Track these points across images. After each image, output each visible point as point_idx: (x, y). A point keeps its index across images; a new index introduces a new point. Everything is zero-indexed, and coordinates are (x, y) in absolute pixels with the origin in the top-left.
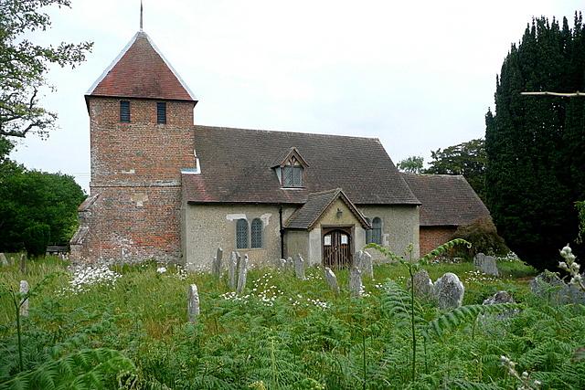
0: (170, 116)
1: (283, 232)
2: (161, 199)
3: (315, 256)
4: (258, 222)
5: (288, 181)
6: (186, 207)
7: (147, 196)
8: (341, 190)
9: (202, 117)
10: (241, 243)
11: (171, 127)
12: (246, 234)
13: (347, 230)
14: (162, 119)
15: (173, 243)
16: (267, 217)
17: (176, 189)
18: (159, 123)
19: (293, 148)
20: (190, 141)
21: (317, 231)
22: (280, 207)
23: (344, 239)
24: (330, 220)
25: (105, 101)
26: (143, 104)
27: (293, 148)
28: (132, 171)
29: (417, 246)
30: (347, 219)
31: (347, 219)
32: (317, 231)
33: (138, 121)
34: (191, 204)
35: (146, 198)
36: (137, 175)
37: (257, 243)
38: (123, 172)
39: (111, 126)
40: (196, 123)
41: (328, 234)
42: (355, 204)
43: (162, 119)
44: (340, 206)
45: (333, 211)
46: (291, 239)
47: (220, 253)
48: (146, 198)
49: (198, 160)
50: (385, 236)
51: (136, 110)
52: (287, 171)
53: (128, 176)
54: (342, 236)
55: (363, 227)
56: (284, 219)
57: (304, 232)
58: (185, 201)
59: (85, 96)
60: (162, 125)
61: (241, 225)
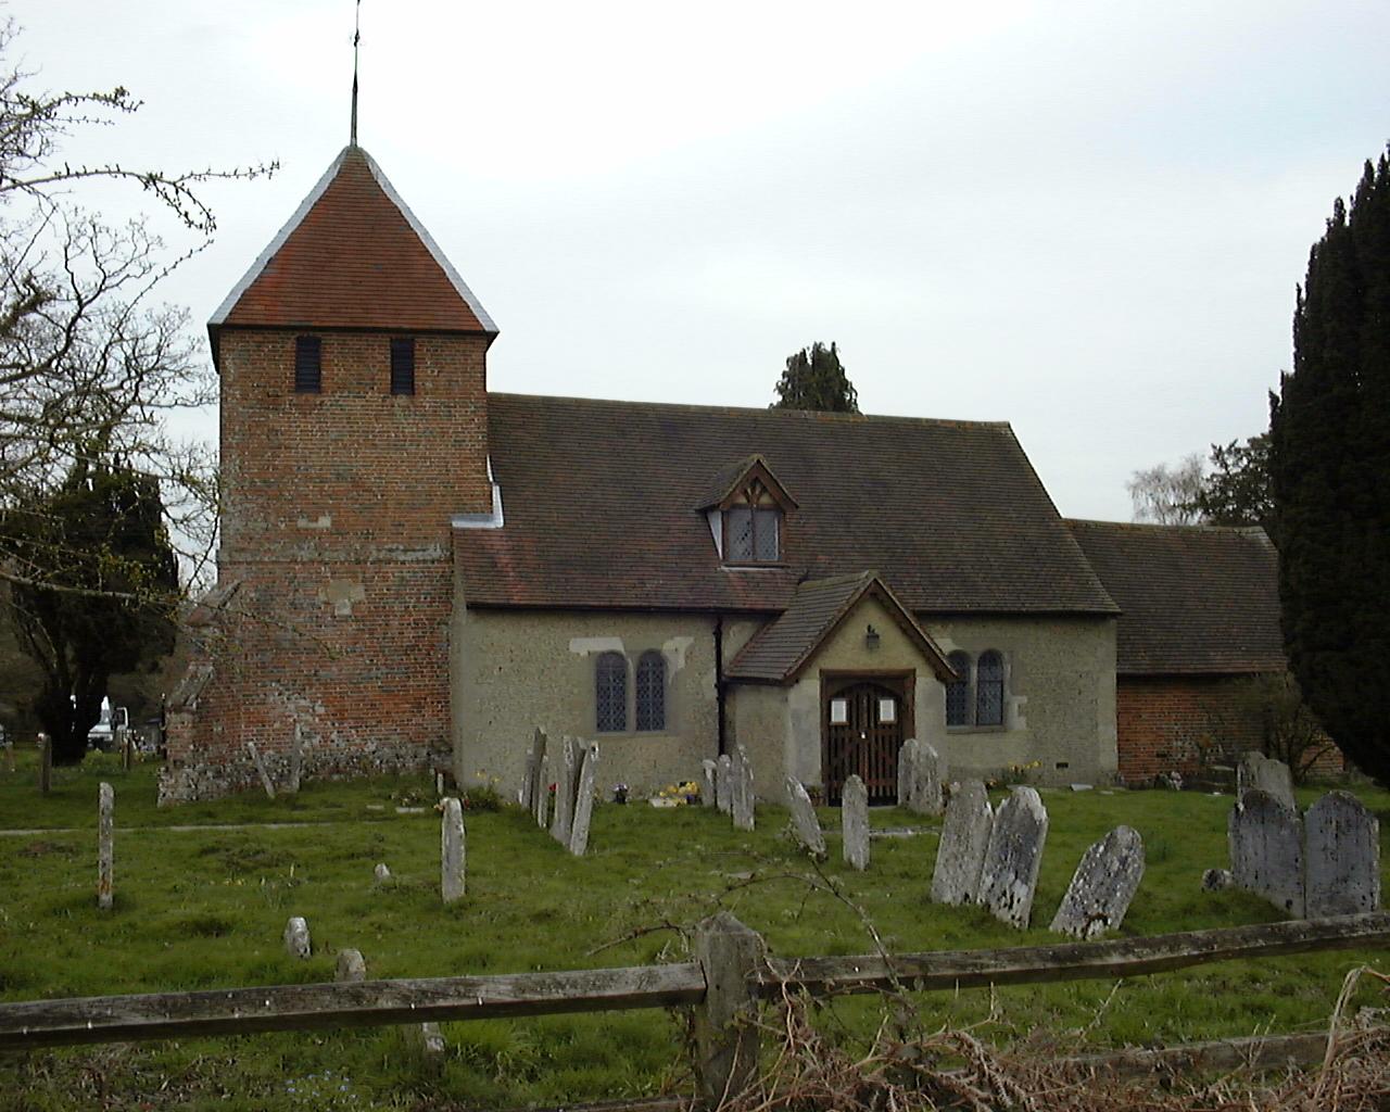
0: (425, 374)
1: (726, 687)
2: (398, 595)
3: (802, 761)
4: (653, 664)
5: (739, 548)
6: (462, 616)
7: (361, 588)
8: (760, 456)
9: (507, 372)
10: (609, 717)
11: (427, 402)
12: (622, 692)
13: (897, 685)
14: (403, 381)
15: (427, 712)
16: (681, 648)
17: (437, 569)
18: (394, 391)
19: (756, 456)
20: (475, 438)
21: (811, 687)
22: (719, 618)
23: (887, 711)
24: (847, 655)
25: (258, 338)
26: (353, 342)
27: (756, 456)
28: (325, 522)
29: (1108, 733)
30: (896, 654)
31: (896, 654)
32: (811, 687)
33: (342, 387)
34: (477, 608)
35: (358, 593)
36: (338, 530)
37: (652, 717)
38: (302, 523)
39: (271, 401)
40: (489, 389)
41: (839, 695)
42: (915, 614)
43: (403, 381)
44: (872, 617)
45: (855, 633)
46: (744, 706)
47: (541, 743)
48: (358, 593)
49: (496, 491)
50: (1015, 702)
51: (1138, 784)
52: (741, 520)
53: (318, 534)
54: (882, 703)
55: (939, 677)
56: (728, 652)
57: (776, 689)
58: (460, 600)
59: (210, 327)
60: (402, 400)
61: (608, 670)
